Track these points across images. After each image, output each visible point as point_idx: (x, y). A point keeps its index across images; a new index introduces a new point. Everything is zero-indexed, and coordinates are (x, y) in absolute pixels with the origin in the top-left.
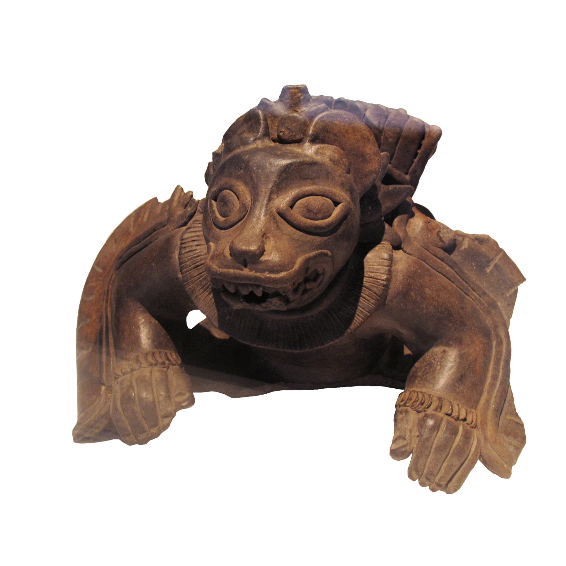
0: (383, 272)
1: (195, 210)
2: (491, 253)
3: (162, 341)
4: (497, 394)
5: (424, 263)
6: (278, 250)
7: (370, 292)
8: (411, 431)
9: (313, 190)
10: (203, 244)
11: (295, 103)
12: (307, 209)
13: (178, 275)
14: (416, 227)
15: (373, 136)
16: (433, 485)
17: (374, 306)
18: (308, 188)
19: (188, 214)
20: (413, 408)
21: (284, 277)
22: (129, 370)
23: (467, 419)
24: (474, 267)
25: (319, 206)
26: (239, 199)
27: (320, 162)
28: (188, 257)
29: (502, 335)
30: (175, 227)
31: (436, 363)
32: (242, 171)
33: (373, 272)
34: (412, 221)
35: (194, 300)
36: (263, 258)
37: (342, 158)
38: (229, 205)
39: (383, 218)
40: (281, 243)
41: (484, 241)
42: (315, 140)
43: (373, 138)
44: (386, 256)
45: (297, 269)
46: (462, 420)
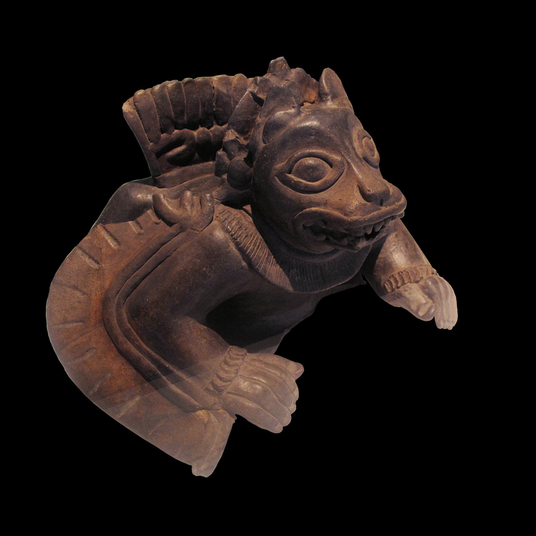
35: (268, 277)
38: (320, 168)
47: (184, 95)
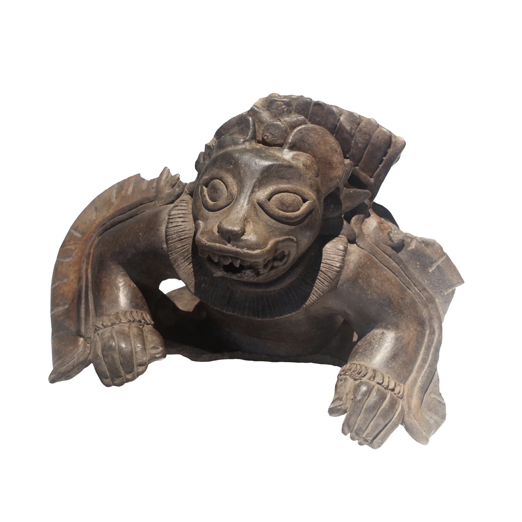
0: (337, 261)
1: (182, 191)
2: (435, 255)
3: (139, 303)
4: (425, 374)
5: (373, 257)
6: (256, 233)
7: (325, 275)
8: (347, 394)
9: (287, 188)
10: (188, 221)
11: (279, 113)
12: (281, 203)
13: (163, 245)
14: (370, 227)
15: (340, 148)
16: (362, 440)
17: (327, 288)
18: (283, 186)
19: (176, 194)
20: (351, 377)
21: (258, 254)
22: (109, 324)
23: (395, 390)
24: (418, 266)
25: (291, 202)
26: (228, 189)
27: (295, 166)
28: (174, 231)
29: (436, 326)
30: (163, 204)
31: (375, 342)
32: (232, 166)
33: (330, 260)
34: (367, 221)
35: (175, 268)
36: (244, 237)
37: (313, 164)
38: (219, 192)
39: (343, 216)
40: (258, 227)
41: (430, 245)
42: (293, 147)
43: (340, 150)
44: (341, 247)
45: (269, 249)
46: (390, 389)
47: (309, 114)
